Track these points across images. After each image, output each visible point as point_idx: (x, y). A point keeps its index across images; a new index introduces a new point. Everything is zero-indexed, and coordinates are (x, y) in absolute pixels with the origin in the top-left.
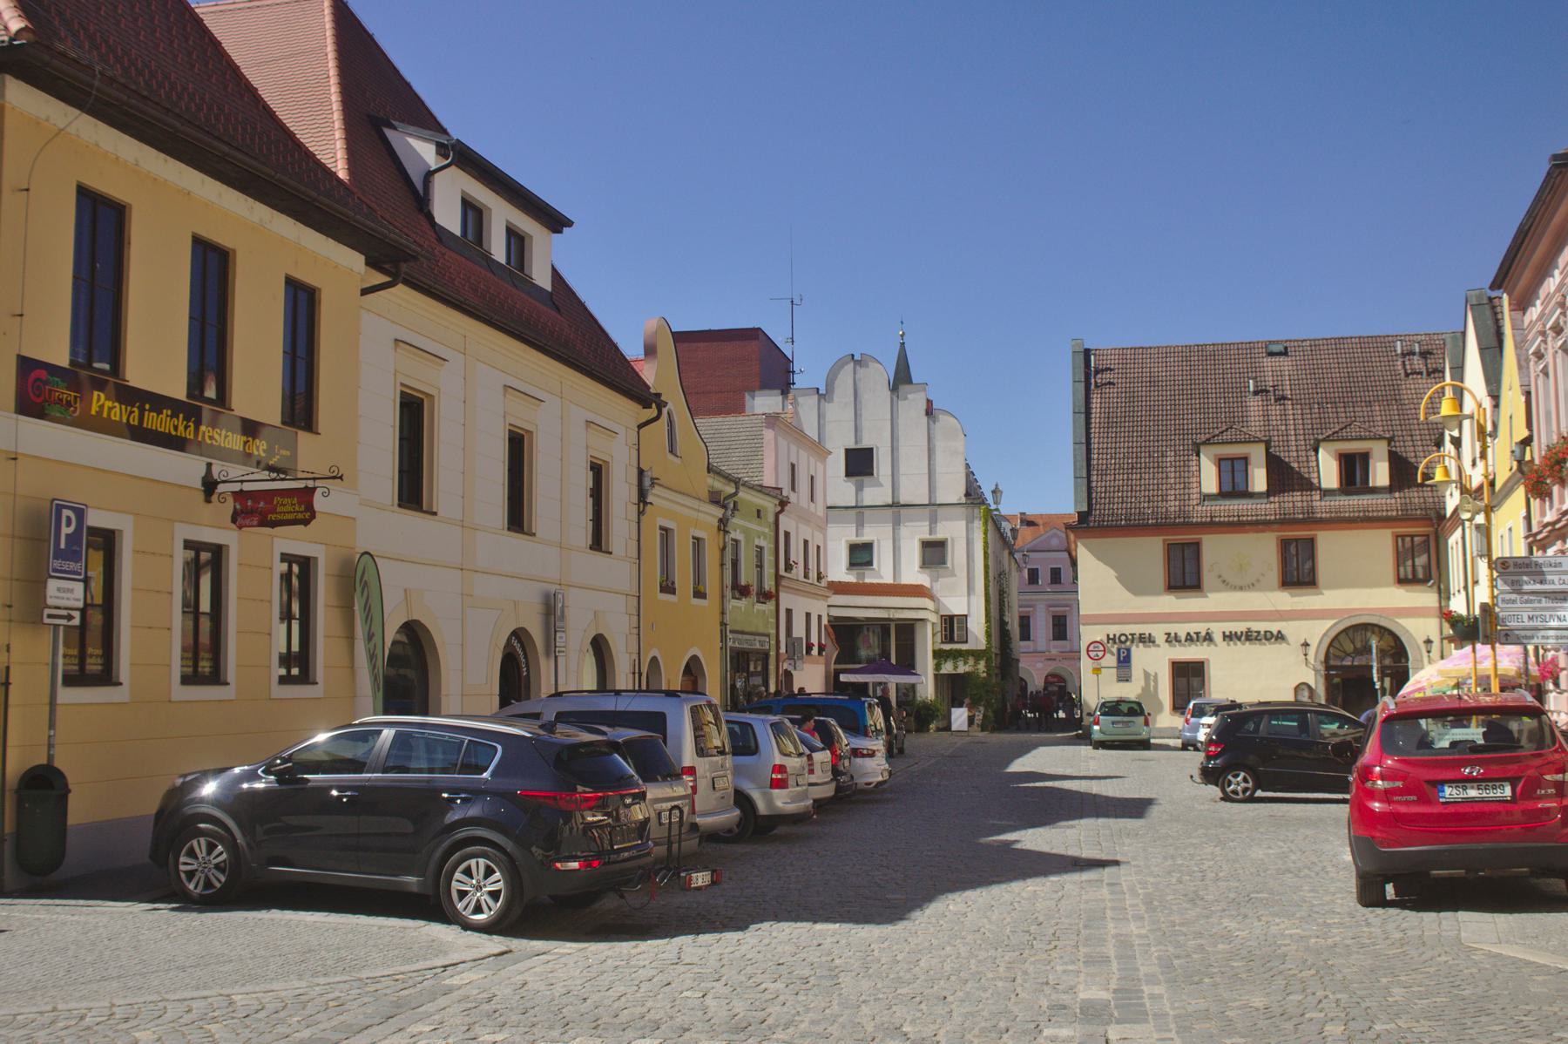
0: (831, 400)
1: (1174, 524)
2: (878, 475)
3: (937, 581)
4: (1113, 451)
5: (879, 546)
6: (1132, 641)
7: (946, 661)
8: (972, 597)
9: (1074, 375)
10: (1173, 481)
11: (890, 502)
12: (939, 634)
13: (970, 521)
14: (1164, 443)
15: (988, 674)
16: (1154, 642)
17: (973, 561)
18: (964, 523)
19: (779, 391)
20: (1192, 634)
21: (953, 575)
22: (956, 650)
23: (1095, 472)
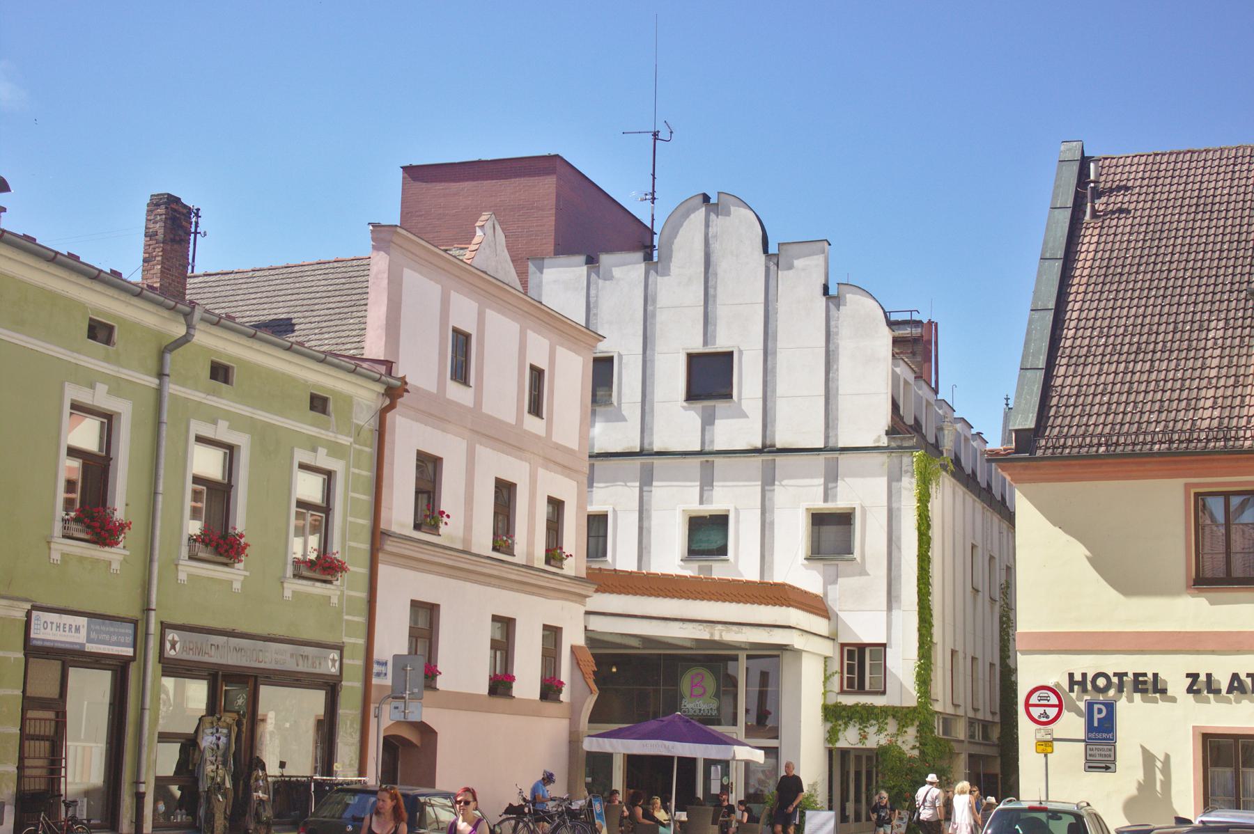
0: (666, 273)
1: (1204, 452)
2: (740, 399)
3: (835, 582)
4: (1106, 323)
5: (737, 522)
6: (1120, 689)
7: (846, 724)
8: (894, 612)
9: (1055, 196)
10: (1214, 373)
11: (759, 445)
12: (836, 678)
13: (894, 478)
14: (1208, 307)
15: (922, 752)
16: (1163, 691)
17: (899, 549)
18: (883, 481)
19: (582, 259)
20: (1243, 677)
21: (863, 572)
22: (864, 707)
23: (1064, 361)
